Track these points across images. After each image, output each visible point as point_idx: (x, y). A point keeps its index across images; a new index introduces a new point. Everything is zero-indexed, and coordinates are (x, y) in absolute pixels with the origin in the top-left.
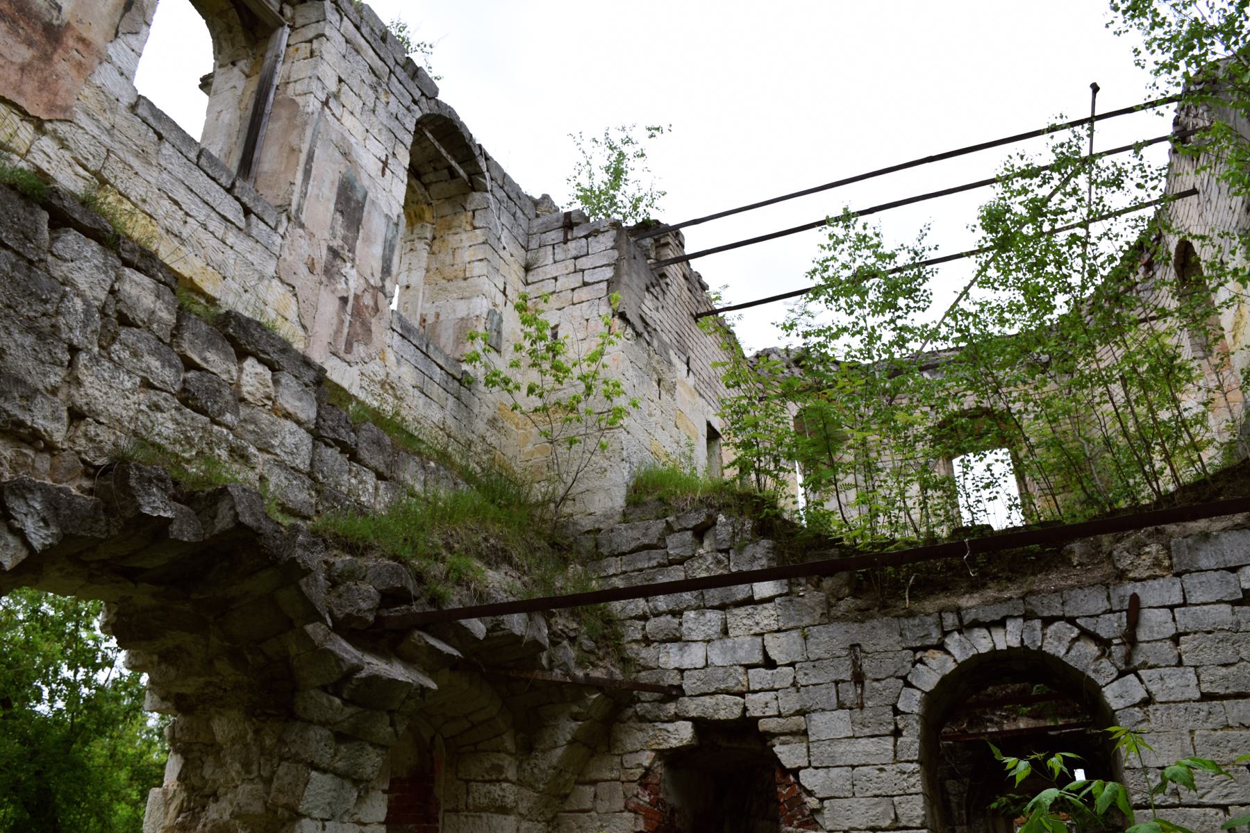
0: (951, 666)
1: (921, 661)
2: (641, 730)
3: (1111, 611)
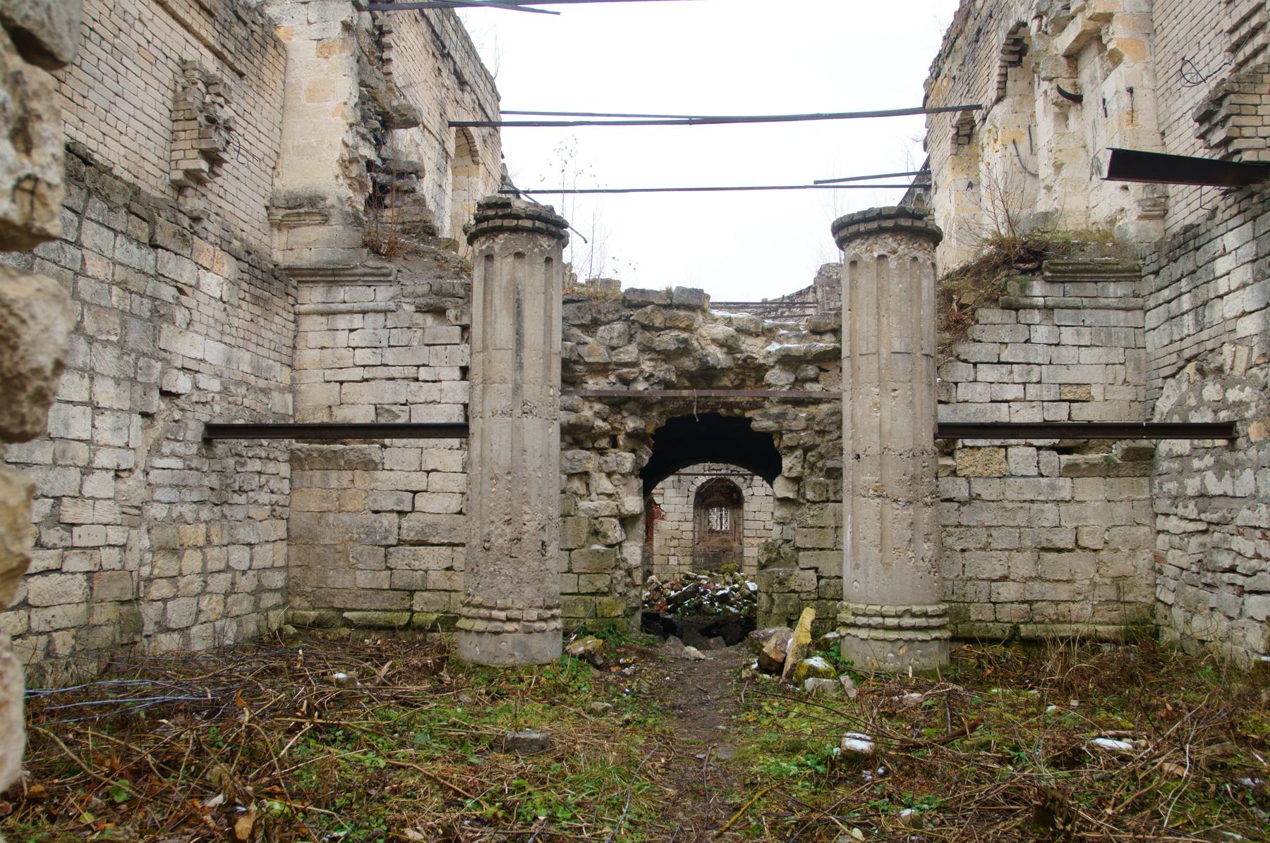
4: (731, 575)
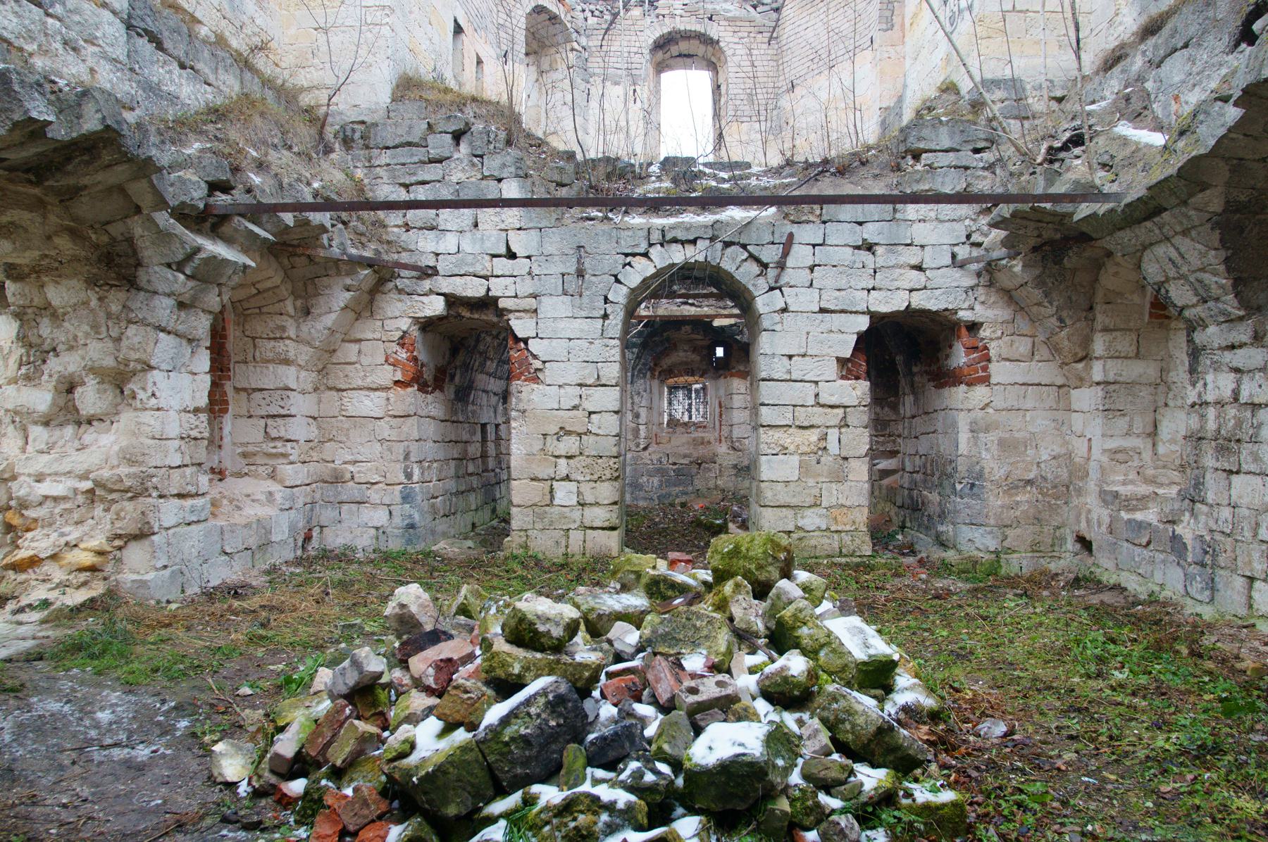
0: (651, 271)
1: (629, 264)
2: (400, 301)
3: (773, 243)
4: (761, 590)
